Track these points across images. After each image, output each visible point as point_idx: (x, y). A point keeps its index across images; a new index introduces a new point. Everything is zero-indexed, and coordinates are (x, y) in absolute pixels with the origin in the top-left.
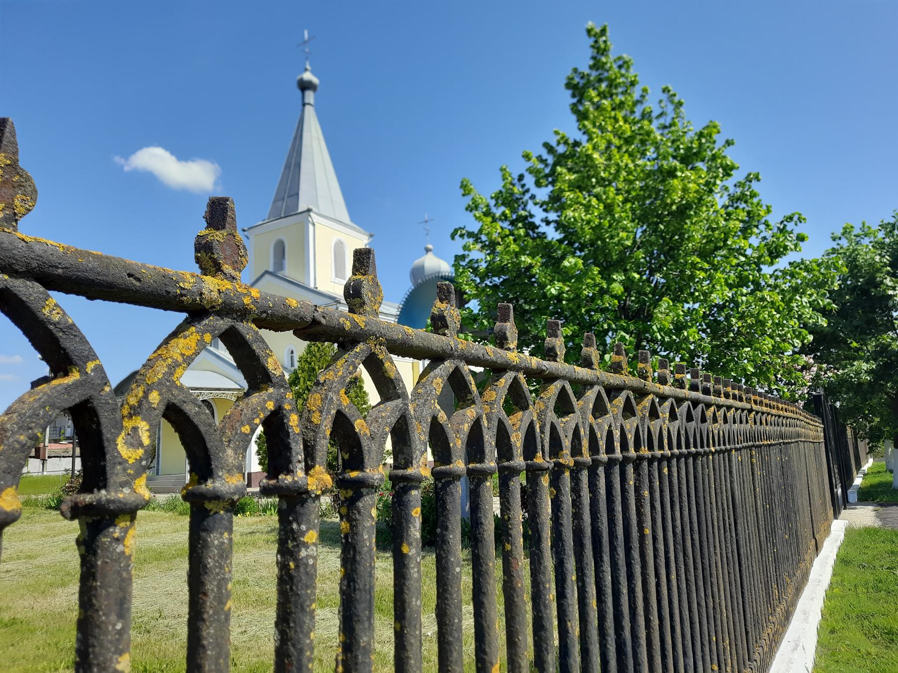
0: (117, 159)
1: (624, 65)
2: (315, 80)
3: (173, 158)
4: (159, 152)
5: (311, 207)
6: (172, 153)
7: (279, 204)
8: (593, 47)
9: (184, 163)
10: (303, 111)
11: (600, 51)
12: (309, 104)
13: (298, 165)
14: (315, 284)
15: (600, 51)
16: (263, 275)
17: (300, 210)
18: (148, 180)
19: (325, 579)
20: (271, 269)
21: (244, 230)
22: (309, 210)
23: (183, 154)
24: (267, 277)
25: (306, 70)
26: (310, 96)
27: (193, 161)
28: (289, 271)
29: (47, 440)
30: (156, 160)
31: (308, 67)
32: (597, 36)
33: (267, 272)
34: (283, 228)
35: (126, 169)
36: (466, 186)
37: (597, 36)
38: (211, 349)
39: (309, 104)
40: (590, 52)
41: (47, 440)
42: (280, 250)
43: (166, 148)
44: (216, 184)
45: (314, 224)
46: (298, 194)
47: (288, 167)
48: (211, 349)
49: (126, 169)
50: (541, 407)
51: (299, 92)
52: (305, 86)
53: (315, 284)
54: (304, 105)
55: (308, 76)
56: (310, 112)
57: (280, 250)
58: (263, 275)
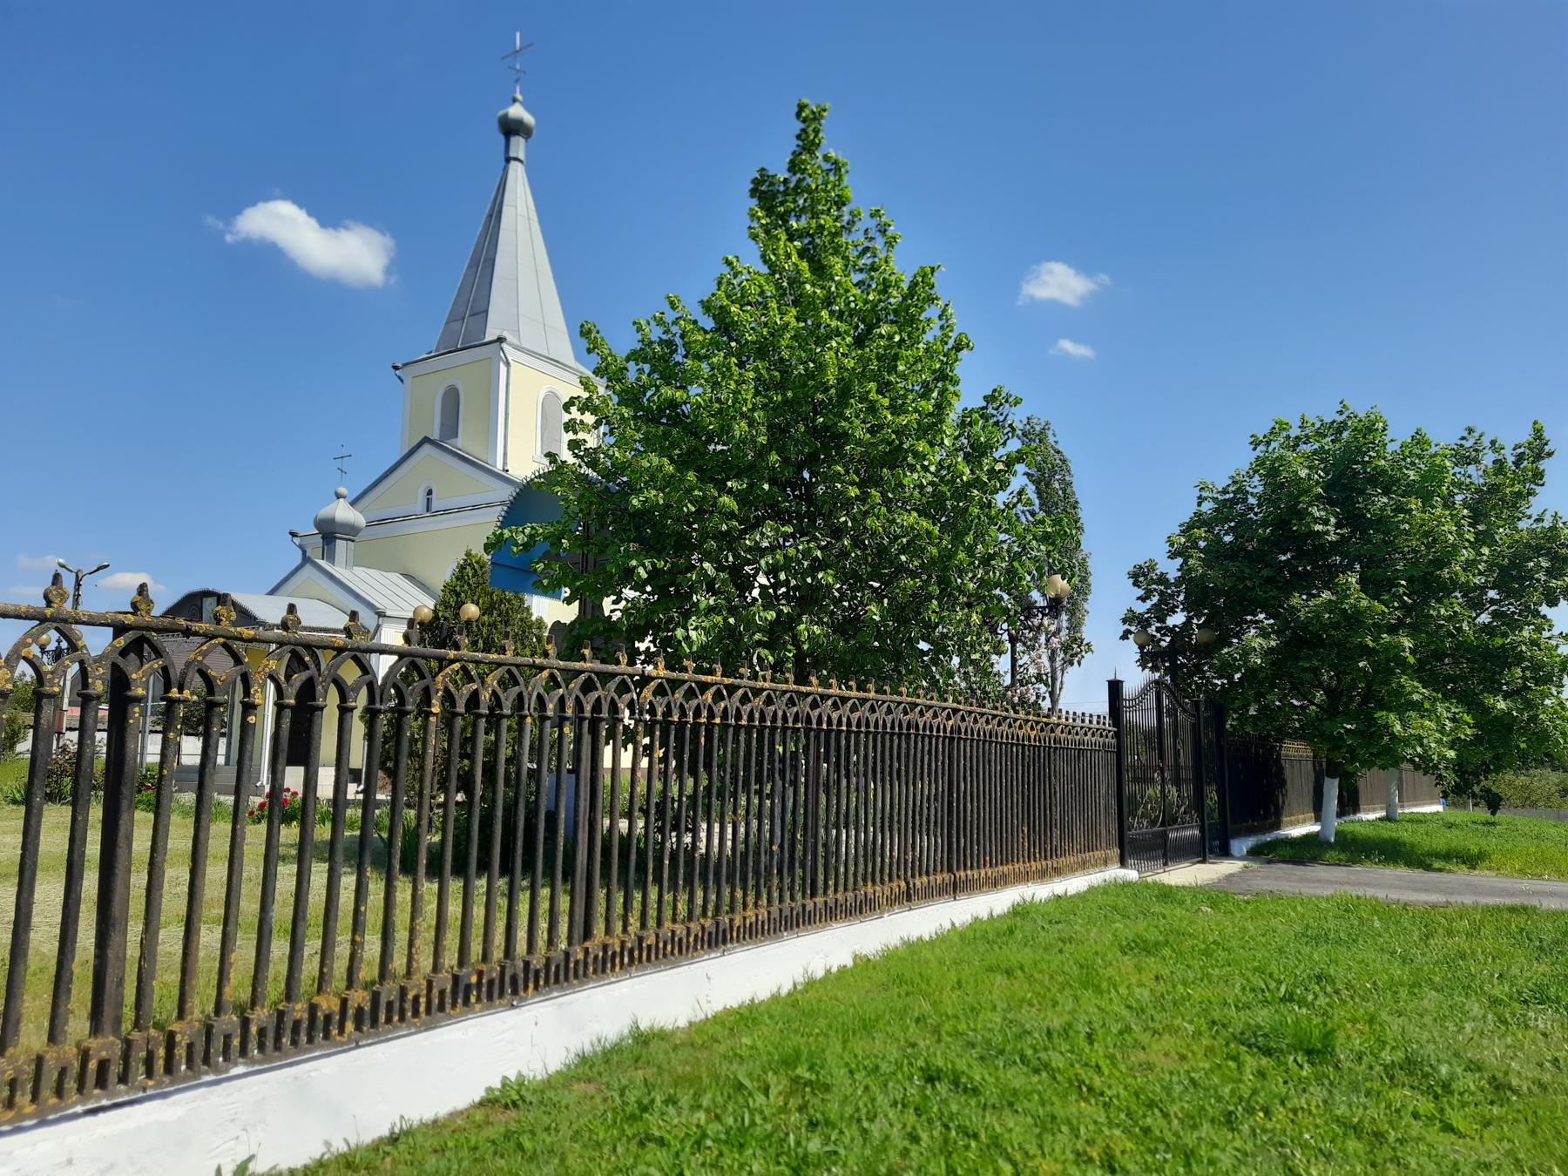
0: (210, 220)
1: (836, 167)
2: (529, 119)
3: (313, 222)
4: (286, 208)
5: (505, 334)
6: (310, 214)
7: (456, 325)
8: (798, 137)
9: (331, 231)
10: (505, 171)
11: (807, 143)
12: (516, 159)
13: (491, 262)
14: (505, 463)
15: (807, 143)
16: (420, 445)
17: (487, 339)
18: (269, 258)
19: (57, 826)
20: (435, 436)
21: (396, 368)
22: (501, 340)
23: (329, 217)
24: (427, 448)
25: (515, 100)
26: (519, 146)
27: (347, 228)
28: (463, 442)
29: (66, 701)
30: (283, 223)
31: (519, 97)
32: (809, 123)
33: (426, 440)
34: (459, 369)
35: (229, 238)
36: (590, 331)
37: (809, 123)
38: (323, 563)
39: (516, 159)
40: (793, 144)
41: (66, 701)
42: (452, 399)
43: (300, 204)
44: (388, 271)
45: (508, 364)
46: (487, 312)
47: (474, 263)
48: (323, 563)
49: (229, 238)
50: (864, 711)
51: (502, 138)
52: (511, 128)
53: (505, 463)
54: (508, 160)
55: (516, 111)
56: (517, 172)
57: (452, 399)
58: (420, 445)
